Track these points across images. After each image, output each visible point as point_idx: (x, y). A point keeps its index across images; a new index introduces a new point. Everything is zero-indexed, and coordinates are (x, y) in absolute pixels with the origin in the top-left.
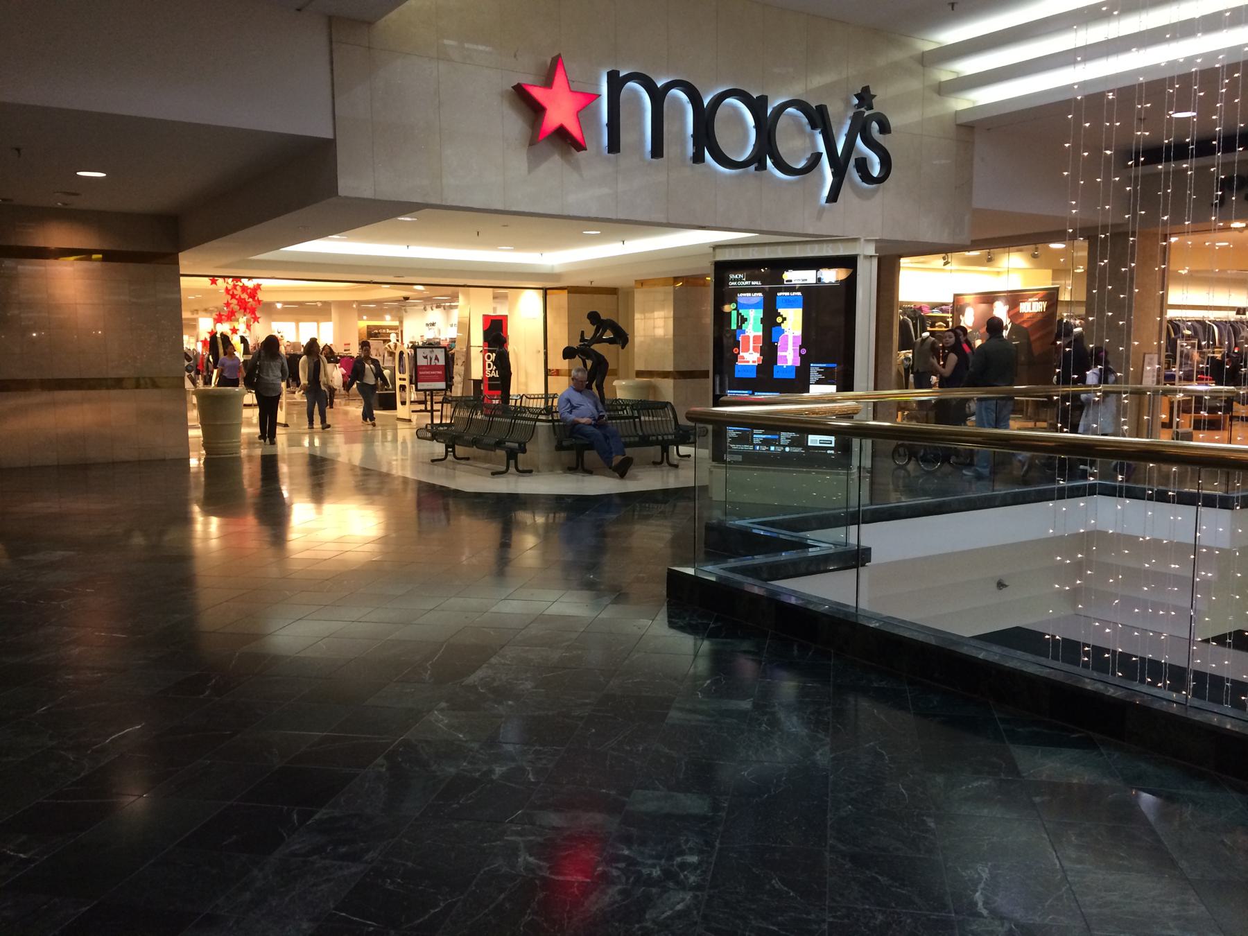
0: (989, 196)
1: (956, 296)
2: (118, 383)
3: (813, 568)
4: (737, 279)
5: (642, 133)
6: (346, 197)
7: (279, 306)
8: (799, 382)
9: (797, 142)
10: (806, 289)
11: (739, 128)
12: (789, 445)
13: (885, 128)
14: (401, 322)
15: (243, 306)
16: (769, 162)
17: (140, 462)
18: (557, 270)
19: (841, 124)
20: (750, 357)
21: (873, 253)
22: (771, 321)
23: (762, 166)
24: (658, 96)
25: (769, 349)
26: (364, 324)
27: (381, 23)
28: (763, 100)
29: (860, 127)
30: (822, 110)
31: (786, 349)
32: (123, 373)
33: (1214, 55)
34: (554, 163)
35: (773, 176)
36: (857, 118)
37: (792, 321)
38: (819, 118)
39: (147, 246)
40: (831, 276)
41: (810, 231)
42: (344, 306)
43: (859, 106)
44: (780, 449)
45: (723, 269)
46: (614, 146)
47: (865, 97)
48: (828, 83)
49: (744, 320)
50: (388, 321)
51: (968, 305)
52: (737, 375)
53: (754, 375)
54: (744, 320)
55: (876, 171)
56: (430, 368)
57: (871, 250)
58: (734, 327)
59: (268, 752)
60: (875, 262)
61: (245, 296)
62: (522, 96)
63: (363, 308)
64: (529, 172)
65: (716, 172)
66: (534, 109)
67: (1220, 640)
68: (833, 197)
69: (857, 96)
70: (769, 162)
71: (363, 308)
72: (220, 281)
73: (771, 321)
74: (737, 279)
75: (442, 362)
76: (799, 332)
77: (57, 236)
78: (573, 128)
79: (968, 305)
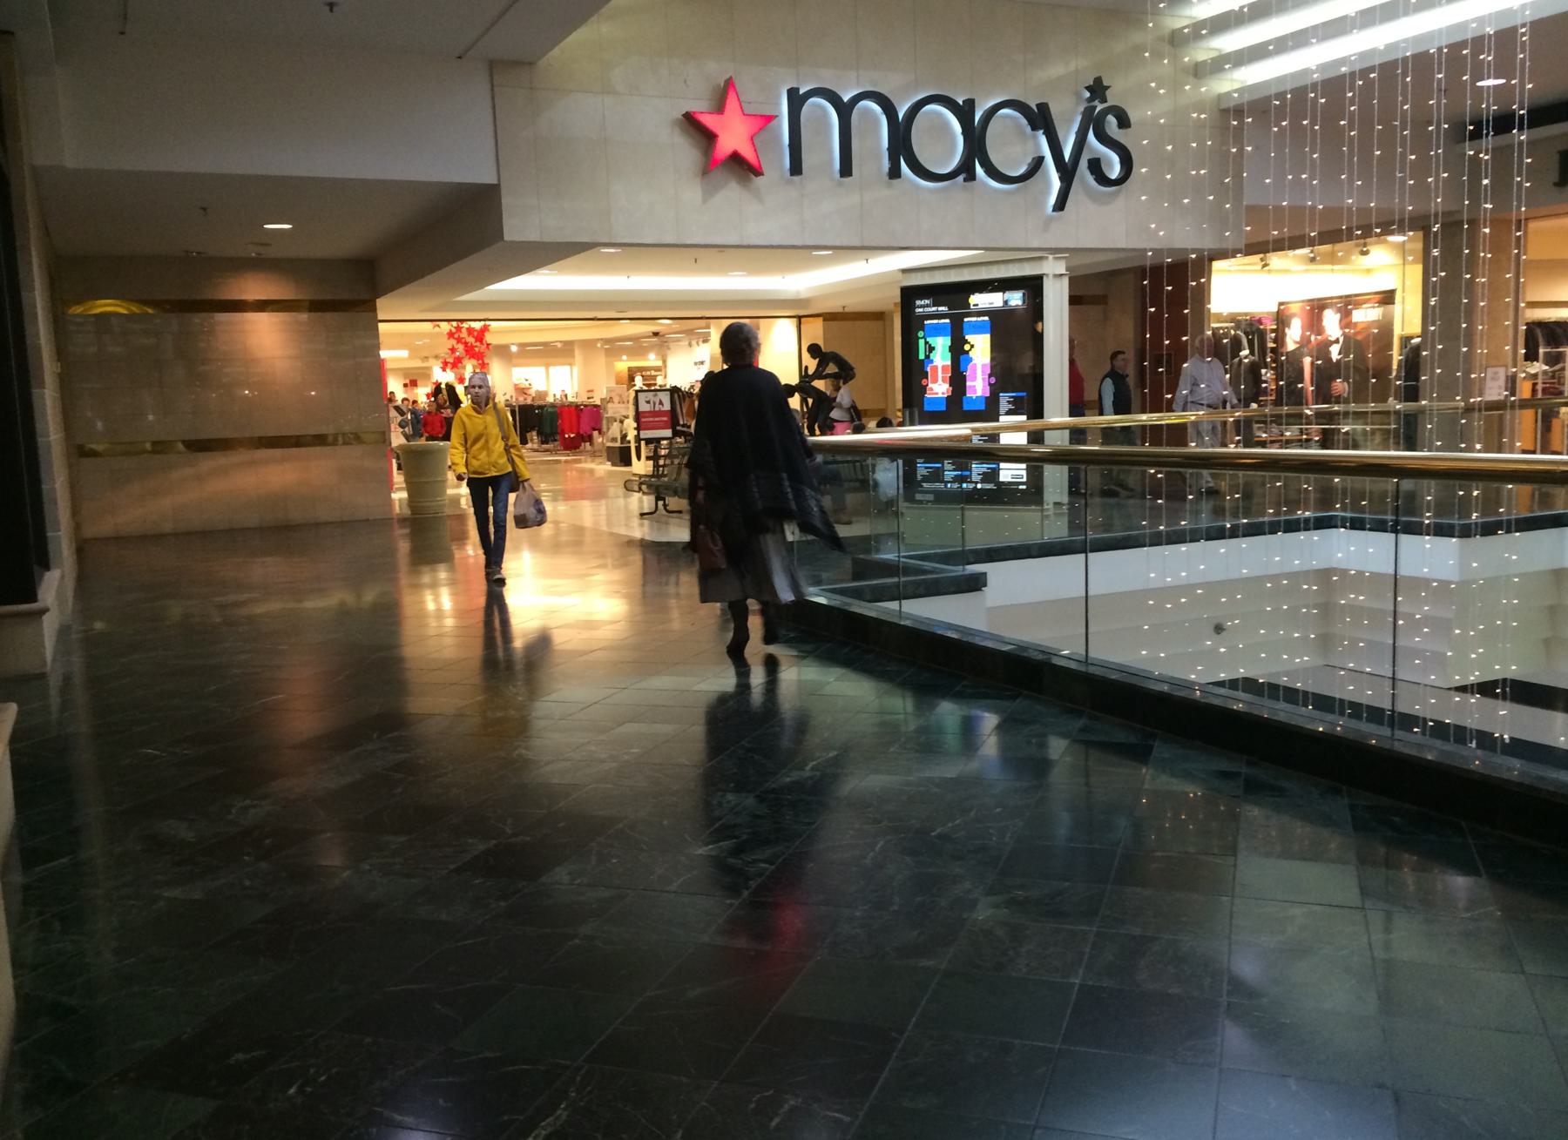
0: (1269, 187)
1: (1281, 304)
2: (320, 440)
3: (922, 590)
4: (923, 306)
5: (831, 151)
6: (512, 242)
7: (514, 349)
8: (989, 411)
9: (1012, 144)
10: (992, 313)
11: (942, 138)
12: (982, 481)
13: (1124, 122)
14: (664, 362)
15: (470, 352)
16: (979, 170)
17: (342, 523)
18: (803, 295)
19: (1070, 121)
20: (939, 389)
21: (1063, 271)
22: (958, 350)
23: (971, 176)
24: (845, 111)
25: (958, 379)
26: (623, 365)
27: (542, 63)
28: (970, 104)
29: (1092, 122)
30: (1043, 107)
31: (974, 379)
32: (323, 430)
33: (1430, 36)
34: (731, 192)
35: (984, 184)
36: (1089, 112)
37: (980, 348)
38: (1040, 119)
39: (345, 293)
40: (1016, 299)
41: (1035, 244)
42: (588, 344)
43: (1090, 100)
44: (971, 486)
45: (910, 295)
46: (796, 168)
47: (1098, 89)
48: (1057, 79)
49: (932, 349)
50: (652, 360)
51: (1294, 315)
52: (927, 408)
53: (943, 408)
54: (932, 349)
55: (1115, 171)
56: (654, 414)
57: (1061, 268)
58: (922, 356)
59: (447, 793)
60: (1066, 281)
61: (471, 340)
62: (691, 122)
63: (613, 348)
64: (705, 201)
65: (918, 187)
66: (707, 137)
67: (1486, 689)
68: (1060, 205)
69: (1088, 88)
70: (979, 170)
71: (613, 348)
72: (443, 325)
73: (958, 350)
74: (923, 306)
75: (667, 407)
76: (987, 360)
77: (254, 288)
78: (747, 152)
79: (1294, 315)
